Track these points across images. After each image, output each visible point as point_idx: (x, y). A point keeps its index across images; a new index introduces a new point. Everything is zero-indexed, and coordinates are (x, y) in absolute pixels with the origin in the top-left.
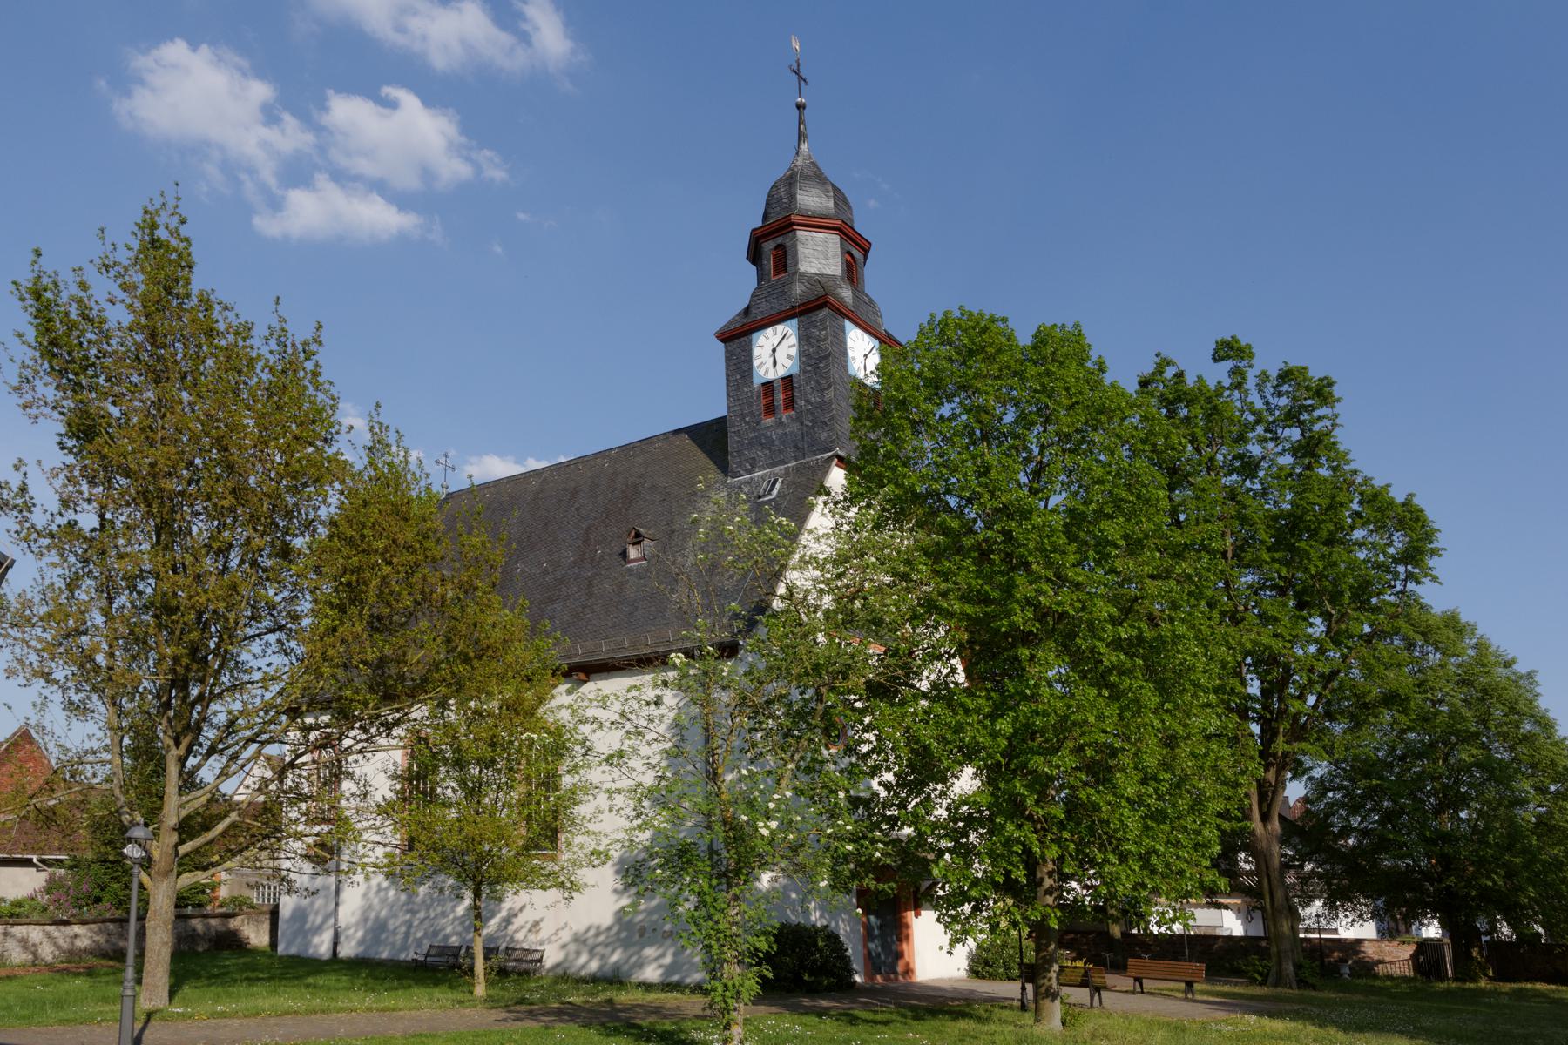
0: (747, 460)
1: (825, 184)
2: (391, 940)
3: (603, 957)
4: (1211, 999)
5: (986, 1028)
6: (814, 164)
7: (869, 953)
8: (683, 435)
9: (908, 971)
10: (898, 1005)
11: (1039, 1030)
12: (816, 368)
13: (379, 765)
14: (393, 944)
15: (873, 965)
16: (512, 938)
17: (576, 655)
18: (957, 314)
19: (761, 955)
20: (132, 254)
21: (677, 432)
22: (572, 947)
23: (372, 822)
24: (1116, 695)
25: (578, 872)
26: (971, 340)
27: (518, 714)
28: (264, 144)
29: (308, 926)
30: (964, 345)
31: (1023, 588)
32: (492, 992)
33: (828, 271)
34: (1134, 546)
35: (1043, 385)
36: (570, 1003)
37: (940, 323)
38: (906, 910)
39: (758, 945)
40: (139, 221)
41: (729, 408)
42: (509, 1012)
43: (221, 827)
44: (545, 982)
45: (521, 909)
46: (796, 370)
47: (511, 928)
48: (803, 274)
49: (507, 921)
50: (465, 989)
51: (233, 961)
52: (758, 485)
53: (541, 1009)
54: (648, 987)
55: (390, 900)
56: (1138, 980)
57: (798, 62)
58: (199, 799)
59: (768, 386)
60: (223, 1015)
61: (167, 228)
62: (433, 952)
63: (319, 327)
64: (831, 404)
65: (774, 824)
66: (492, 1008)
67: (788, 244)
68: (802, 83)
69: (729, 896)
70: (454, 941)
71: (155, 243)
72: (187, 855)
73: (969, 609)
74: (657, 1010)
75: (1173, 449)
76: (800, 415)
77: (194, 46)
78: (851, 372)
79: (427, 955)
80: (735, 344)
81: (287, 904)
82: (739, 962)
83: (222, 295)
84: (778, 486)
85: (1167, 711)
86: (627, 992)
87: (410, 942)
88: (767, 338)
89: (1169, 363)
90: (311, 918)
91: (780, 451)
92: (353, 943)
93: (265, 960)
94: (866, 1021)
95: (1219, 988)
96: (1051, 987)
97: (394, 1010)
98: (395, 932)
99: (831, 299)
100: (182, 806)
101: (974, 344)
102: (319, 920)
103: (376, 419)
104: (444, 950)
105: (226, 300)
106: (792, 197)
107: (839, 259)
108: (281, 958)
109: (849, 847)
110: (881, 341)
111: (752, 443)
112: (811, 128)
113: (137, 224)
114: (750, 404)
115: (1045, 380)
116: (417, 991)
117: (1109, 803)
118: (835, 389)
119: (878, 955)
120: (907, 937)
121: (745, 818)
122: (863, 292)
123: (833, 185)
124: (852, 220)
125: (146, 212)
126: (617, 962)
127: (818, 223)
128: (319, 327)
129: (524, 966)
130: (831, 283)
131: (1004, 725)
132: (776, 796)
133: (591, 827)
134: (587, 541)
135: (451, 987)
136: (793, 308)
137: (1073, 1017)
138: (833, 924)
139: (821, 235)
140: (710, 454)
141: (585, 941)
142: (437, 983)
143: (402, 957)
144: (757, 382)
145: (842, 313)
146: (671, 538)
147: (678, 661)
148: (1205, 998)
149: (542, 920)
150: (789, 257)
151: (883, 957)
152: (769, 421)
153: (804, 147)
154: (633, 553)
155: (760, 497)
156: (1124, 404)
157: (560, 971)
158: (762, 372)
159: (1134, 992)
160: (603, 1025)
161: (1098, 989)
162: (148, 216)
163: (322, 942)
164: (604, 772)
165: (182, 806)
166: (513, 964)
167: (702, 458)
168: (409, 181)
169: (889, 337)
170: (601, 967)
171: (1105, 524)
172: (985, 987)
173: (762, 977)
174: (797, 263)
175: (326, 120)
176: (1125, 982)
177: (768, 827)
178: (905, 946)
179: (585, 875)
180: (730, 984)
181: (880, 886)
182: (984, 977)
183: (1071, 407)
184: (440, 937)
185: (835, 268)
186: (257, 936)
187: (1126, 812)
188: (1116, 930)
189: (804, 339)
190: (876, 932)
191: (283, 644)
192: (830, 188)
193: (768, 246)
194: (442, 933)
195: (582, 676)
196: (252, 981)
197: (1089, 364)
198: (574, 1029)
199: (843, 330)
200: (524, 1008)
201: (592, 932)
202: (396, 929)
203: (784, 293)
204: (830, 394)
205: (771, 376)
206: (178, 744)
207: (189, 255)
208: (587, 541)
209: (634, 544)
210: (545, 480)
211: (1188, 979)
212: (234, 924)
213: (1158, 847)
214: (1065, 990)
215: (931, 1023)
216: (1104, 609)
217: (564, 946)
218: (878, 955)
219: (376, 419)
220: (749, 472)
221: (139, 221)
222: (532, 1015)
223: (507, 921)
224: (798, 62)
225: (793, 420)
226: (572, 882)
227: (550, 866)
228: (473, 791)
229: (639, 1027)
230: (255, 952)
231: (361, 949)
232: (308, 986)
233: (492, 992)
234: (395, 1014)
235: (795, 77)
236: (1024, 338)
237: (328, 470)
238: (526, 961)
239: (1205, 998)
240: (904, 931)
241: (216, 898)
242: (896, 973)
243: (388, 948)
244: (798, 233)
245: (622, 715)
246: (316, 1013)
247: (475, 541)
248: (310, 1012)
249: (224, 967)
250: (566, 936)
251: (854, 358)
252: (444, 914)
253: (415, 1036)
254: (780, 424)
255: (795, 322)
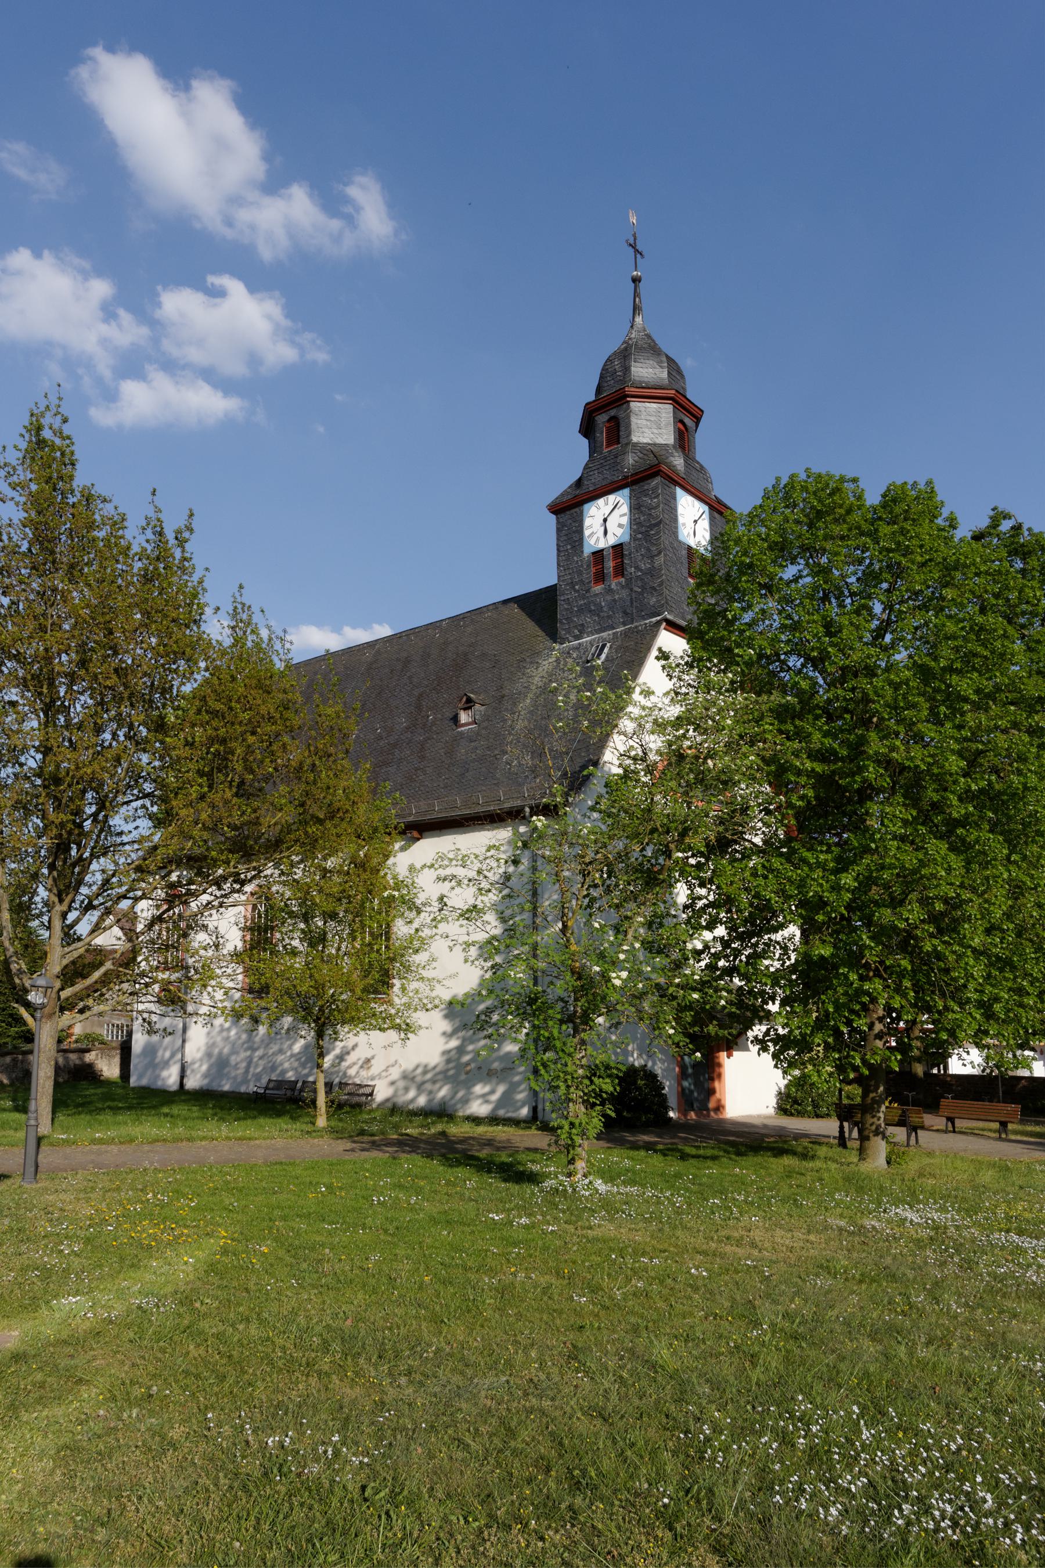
0: (575, 627)
1: (659, 355)
2: (233, 1074)
3: (430, 1092)
4: (1025, 1139)
5: (811, 1164)
6: (649, 336)
7: (683, 1089)
8: (512, 604)
9: (719, 1108)
10: (719, 1141)
11: (866, 1167)
12: (647, 536)
13: (233, 920)
14: (235, 1078)
15: (687, 1102)
16: (345, 1073)
17: (410, 814)
18: (803, 476)
19: (604, 1095)
20: (20, 455)
21: (505, 602)
22: (401, 1084)
23: (224, 969)
24: (960, 847)
25: (414, 1015)
26: (820, 501)
27: (365, 871)
28: (104, 342)
29: (157, 1060)
30: (813, 508)
31: (875, 745)
32: (333, 1123)
33: (660, 441)
34: (984, 699)
35: (898, 544)
36: (407, 1135)
37: (785, 486)
38: (719, 1051)
39: (604, 1087)
40: (27, 424)
41: (559, 577)
42: (354, 1142)
43: (97, 975)
44: (377, 1115)
45: (353, 1048)
46: (626, 538)
47: (344, 1064)
48: (636, 445)
49: (341, 1058)
50: (307, 1119)
51: (92, 1091)
52: (586, 651)
53: (382, 1140)
54: (476, 1120)
55: (232, 1038)
56: (951, 1120)
57: (634, 236)
58: (78, 950)
59: (599, 555)
60: (100, 1141)
61: (51, 428)
62: (271, 1085)
63: (191, 515)
64: (660, 570)
65: (624, 974)
66: (338, 1138)
67: (621, 415)
68: (638, 256)
69: (576, 1040)
70: (290, 1076)
71: (41, 443)
72: (67, 999)
73: (819, 768)
74: (489, 1143)
75: (1027, 603)
76: (629, 581)
77: (38, 255)
78: (681, 538)
79: (266, 1088)
80: (566, 517)
81: (139, 1040)
82: (584, 1102)
83: (99, 490)
84: (606, 650)
85: (1015, 862)
86: (456, 1124)
87: (250, 1077)
88: (599, 508)
89: (1007, 516)
90: (160, 1053)
91: (609, 617)
92: (199, 1076)
93: (120, 1091)
94: (694, 1157)
95: (1029, 1128)
96: (880, 1125)
97: (250, 1139)
98: (236, 1067)
99: (664, 468)
100: (63, 956)
101: (824, 506)
102: (167, 1054)
103: (239, 600)
104: (280, 1084)
105: (104, 492)
106: (627, 369)
107: (671, 428)
108: (134, 1089)
109: (696, 996)
110: (712, 508)
111: (581, 610)
112: (645, 302)
113: (25, 427)
114: (580, 573)
115: (901, 538)
116: (262, 1120)
117: (954, 952)
118: (665, 555)
119: (691, 1092)
120: (720, 1076)
121: (597, 969)
122: (694, 459)
123: (667, 357)
124: (684, 389)
125: (32, 415)
126: (444, 1097)
127: (651, 393)
128: (191, 515)
129: (356, 1099)
130: (663, 452)
131: (847, 879)
132: (625, 948)
133: (425, 973)
134: (419, 708)
135: (294, 1119)
136: (626, 478)
137: (898, 1156)
138: (650, 1064)
139: (654, 405)
140: (539, 623)
141: (414, 1077)
142: (279, 1114)
143: (243, 1089)
144: (587, 551)
145: (674, 480)
146: (501, 701)
147: (539, 824)
148: (1019, 1138)
149: (373, 1057)
150: (622, 429)
151: (696, 1094)
152: (598, 588)
153: (639, 320)
154: (464, 717)
155: (588, 662)
156: (978, 560)
157: (389, 1105)
158: (592, 542)
159: (946, 1131)
160: (443, 1156)
161: (914, 1129)
162: (34, 419)
163: (170, 1076)
164: (461, 926)
165: (63, 956)
166: (346, 1097)
167: (531, 627)
168: (236, 368)
169: (719, 501)
170: (430, 1101)
171: (955, 679)
172: (795, 1124)
173: (605, 1115)
174: (629, 434)
175: (158, 314)
176: (939, 1122)
177: (618, 977)
178: (716, 1084)
179: (420, 1018)
180: (577, 1122)
181: (721, 1033)
182: (792, 1115)
183: (923, 565)
184: (278, 1072)
185: (667, 437)
186: (109, 1069)
187: (972, 962)
188: (919, 1069)
189: (635, 508)
190: (690, 1071)
191: (147, 809)
192: (664, 359)
193: (602, 419)
194: (280, 1068)
195: (416, 834)
196: (115, 1110)
197: (939, 521)
198: (418, 1159)
199: (674, 497)
200: (366, 1138)
201: (419, 1070)
202: (237, 1064)
203: (616, 463)
204: (660, 560)
205: (602, 545)
206: (61, 901)
207: (72, 453)
208: (419, 708)
209: (465, 709)
210: (378, 652)
211: (1003, 1119)
212: (89, 1057)
213: (1002, 994)
214: (891, 1130)
215: (752, 1160)
216: (955, 764)
217: (393, 1083)
218: (691, 1092)
219: (239, 600)
220: (577, 638)
221: (27, 424)
222: (375, 1145)
223: (341, 1058)
224: (634, 236)
225: (623, 587)
226: (407, 1025)
227: (379, 1008)
228: (316, 940)
229: (477, 1159)
230: (108, 1083)
231: (206, 1081)
232: (166, 1115)
233: (333, 1123)
234: (252, 1143)
235: (632, 250)
236: (873, 498)
237: (199, 646)
238: (358, 1095)
239: (1019, 1138)
240: (717, 1069)
241: (72, 1035)
242: (708, 1110)
243: (231, 1081)
244: (632, 404)
245: (479, 872)
246: (182, 1140)
247: (329, 711)
248: (177, 1140)
249: (86, 1096)
250: (395, 1074)
251: (684, 524)
252: (281, 1051)
253: (276, 1163)
254: (609, 590)
255: (626, 492)
